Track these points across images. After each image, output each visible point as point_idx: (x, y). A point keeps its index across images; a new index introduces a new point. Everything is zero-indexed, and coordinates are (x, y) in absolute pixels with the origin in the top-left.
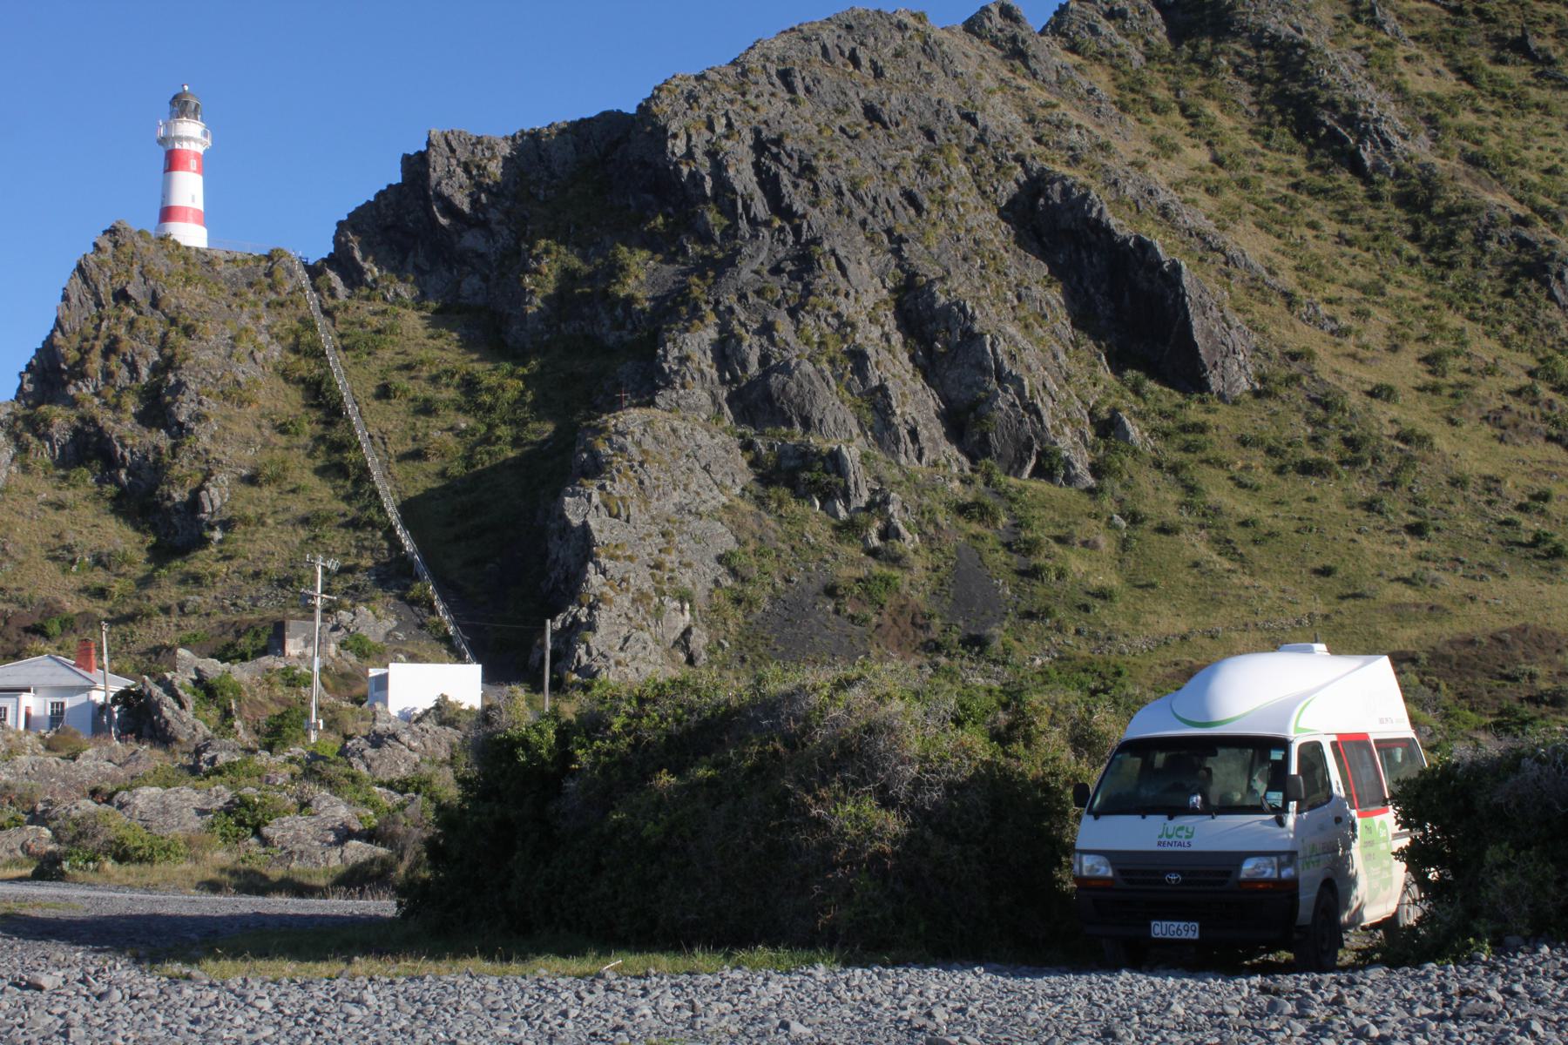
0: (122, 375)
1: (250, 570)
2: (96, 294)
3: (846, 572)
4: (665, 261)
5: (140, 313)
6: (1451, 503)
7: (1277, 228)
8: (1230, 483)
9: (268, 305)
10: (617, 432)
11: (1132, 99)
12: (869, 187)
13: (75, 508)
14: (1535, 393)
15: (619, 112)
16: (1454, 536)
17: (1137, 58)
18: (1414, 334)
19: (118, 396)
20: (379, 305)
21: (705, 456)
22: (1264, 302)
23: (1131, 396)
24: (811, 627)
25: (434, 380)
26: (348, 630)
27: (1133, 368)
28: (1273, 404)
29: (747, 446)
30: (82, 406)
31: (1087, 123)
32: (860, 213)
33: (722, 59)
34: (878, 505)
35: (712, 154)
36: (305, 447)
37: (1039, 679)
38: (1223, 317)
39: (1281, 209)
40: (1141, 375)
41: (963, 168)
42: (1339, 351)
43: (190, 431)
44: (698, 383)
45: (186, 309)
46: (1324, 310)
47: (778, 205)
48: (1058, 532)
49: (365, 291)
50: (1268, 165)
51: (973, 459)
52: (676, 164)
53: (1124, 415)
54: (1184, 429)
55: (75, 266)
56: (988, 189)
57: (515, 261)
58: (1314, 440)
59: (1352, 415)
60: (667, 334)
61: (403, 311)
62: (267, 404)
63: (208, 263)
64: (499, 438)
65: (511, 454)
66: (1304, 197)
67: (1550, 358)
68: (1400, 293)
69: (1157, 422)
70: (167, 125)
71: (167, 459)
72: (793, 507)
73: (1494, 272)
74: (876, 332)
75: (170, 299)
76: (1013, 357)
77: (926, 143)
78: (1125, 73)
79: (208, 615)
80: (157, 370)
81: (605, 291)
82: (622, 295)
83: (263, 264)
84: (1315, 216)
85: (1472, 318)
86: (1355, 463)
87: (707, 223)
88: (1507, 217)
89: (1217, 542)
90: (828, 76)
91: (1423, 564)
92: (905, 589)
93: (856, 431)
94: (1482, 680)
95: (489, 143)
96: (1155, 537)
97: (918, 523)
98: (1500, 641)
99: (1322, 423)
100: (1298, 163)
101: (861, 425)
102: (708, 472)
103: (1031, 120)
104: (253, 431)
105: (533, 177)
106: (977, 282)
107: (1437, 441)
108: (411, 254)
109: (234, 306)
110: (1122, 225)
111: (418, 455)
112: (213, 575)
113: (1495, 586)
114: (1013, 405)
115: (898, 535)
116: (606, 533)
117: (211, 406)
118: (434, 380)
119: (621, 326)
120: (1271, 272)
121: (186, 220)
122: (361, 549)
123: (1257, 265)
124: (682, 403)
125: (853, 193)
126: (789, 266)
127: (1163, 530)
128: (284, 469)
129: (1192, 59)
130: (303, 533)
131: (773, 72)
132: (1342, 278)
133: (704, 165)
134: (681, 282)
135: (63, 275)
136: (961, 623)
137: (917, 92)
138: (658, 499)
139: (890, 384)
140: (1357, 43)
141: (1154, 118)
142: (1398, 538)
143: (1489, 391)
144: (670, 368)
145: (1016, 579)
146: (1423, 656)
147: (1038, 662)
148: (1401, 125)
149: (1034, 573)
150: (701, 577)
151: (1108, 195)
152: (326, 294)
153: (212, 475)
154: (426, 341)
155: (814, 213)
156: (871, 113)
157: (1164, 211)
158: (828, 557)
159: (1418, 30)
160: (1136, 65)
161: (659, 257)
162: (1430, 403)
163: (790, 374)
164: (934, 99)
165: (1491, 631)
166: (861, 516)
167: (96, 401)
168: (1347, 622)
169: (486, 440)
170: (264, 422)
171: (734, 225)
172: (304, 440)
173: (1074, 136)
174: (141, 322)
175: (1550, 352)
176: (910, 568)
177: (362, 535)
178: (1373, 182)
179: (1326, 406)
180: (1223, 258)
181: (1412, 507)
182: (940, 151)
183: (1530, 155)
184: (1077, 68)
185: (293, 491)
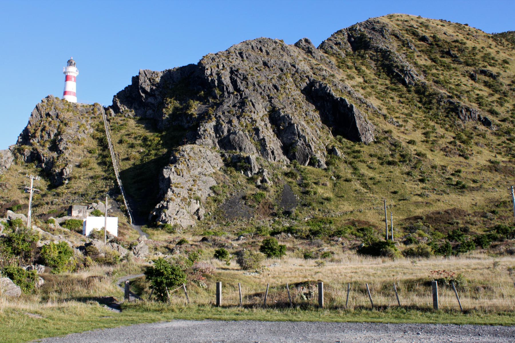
0: (46, 137)
1: (74, 192)
2: (41, 114)
3: (250, 192)
4: (203, 104)
5: (53, 119)
6: (432, 173)
7: (381, 98)
8: (367, 167)
10: (182, 151)
11: (342, 64)
12: (262, 84)
14: (455, 143)
16: (433, 182)
17: (343, 55)
18: (421, 127)
19: (44, 143)
20: (123, 118)
21: (209, 158)
22: (378, 117)
23: (338, 143)
24: (237, 209)
25: (135, 138)
27: (339, 135)
28: (379, 145)
29: (223, 156)
31: (328, 69)
32: (260, 90)
33: (223, 50)
34: (260, 173)
35: (218, 74)
36: (96, 157)
37: (306, 224)
38: (365, 120)
39: (383, 94)
40: (341, 137)
41: (291, 79)
42: (399, 131)
43: (63, 152)
46: (395, 120)
47: (236, 88)
48: (315, 181)
49: (120, 114)
50: (380, 83)
51: (291, 160)
52: (207, 77)
53: (336, 148)
54: (354, 152)
56: (298, 85)
57: (162, 105)
58: (392, 155)
59: (403, 148)
61: (129, 120)
65: (153, 158)
66: (389, 91)
67: (459, 134)
68: (416, 116)
69: (346, 150)
70: (66, 68)
71: (56, 160)
72: (235, 173)
73: (443, 111)
74: (263, 123)
75: (62, 116)
76: (303, 130)
77: (281, 72)
78: (340, 59)
80: (56, 135)
81: (185, 112)
84: (393, 96)
85: (437, 123)
86: (404, 161)
87: (215, 93)
88: (446, 96)
89: (363, 184)
90: (253, 54)
91: (424, 190)
92: (267, 197)
93: (255, 151)
94: (442, 224)
96: (344, 183)
97: (273, 178)
98: (447, 213)
99: (394, 150)
100: (388, 82)
101: (257, 150)
103: (312, 68)
104: (81, 152)
105: (168, 82)
106: (294, 110)
107: (428, 156)
110: (337, 95)
111: (128, 159)
112: (63, 193)
113: (445, 196)
114: (303, 144)
115: (266, 182)
116: (175, 180)
117: (70, 146)
118: (135, 138)
119: (189, 122)
120: (380, 109)
121: (70, 94)
122: (106, 186)
123: (376, 107)
125: (258, 85)
126: (238, 105)
127: (347, 180)
128: (89, 163)
129: (359, 55)
130: (91, 181)
131: (237, 53)
132: (400, 112)
133: (215, 77)
135: (32, 109)
136: (283, 207)
137: (279, 59)
139: (266, 138)
140: (404, 52)
141: (348, 70)
142: (417, 183)
143: (442, 143)
145: (301, 195)
146: (424, 217)
147: (306, 219)
148: (416, 72)
149: (307, 193)
150: (204, 193)
151: (334, 88)
155: (247, 91)
156: (265, 64)
157: (349, 92)
158: (244, 188)
159: (421, 49)
160: (343, 57)
161: (202, 103)
162: (425, 145)
163: (236, 134)
164: (284, 61)
165: (444, 210)
166: (256, 176)
167: (38, 144)
168: (401, 207)
169: (147, 155)
171: (223, 94)
172: (96, 155)
173: (324, 73)
174: (53, 122)
175: (459, 132)
176: (269, 191)
177: (107, 182)
178: (408, 87)
179: (395, 146)
180: (366, 105)
181: (421, 174)
182: (285, 74)
183: (452, 81)
184: (327, 57)
185: (90, 169)
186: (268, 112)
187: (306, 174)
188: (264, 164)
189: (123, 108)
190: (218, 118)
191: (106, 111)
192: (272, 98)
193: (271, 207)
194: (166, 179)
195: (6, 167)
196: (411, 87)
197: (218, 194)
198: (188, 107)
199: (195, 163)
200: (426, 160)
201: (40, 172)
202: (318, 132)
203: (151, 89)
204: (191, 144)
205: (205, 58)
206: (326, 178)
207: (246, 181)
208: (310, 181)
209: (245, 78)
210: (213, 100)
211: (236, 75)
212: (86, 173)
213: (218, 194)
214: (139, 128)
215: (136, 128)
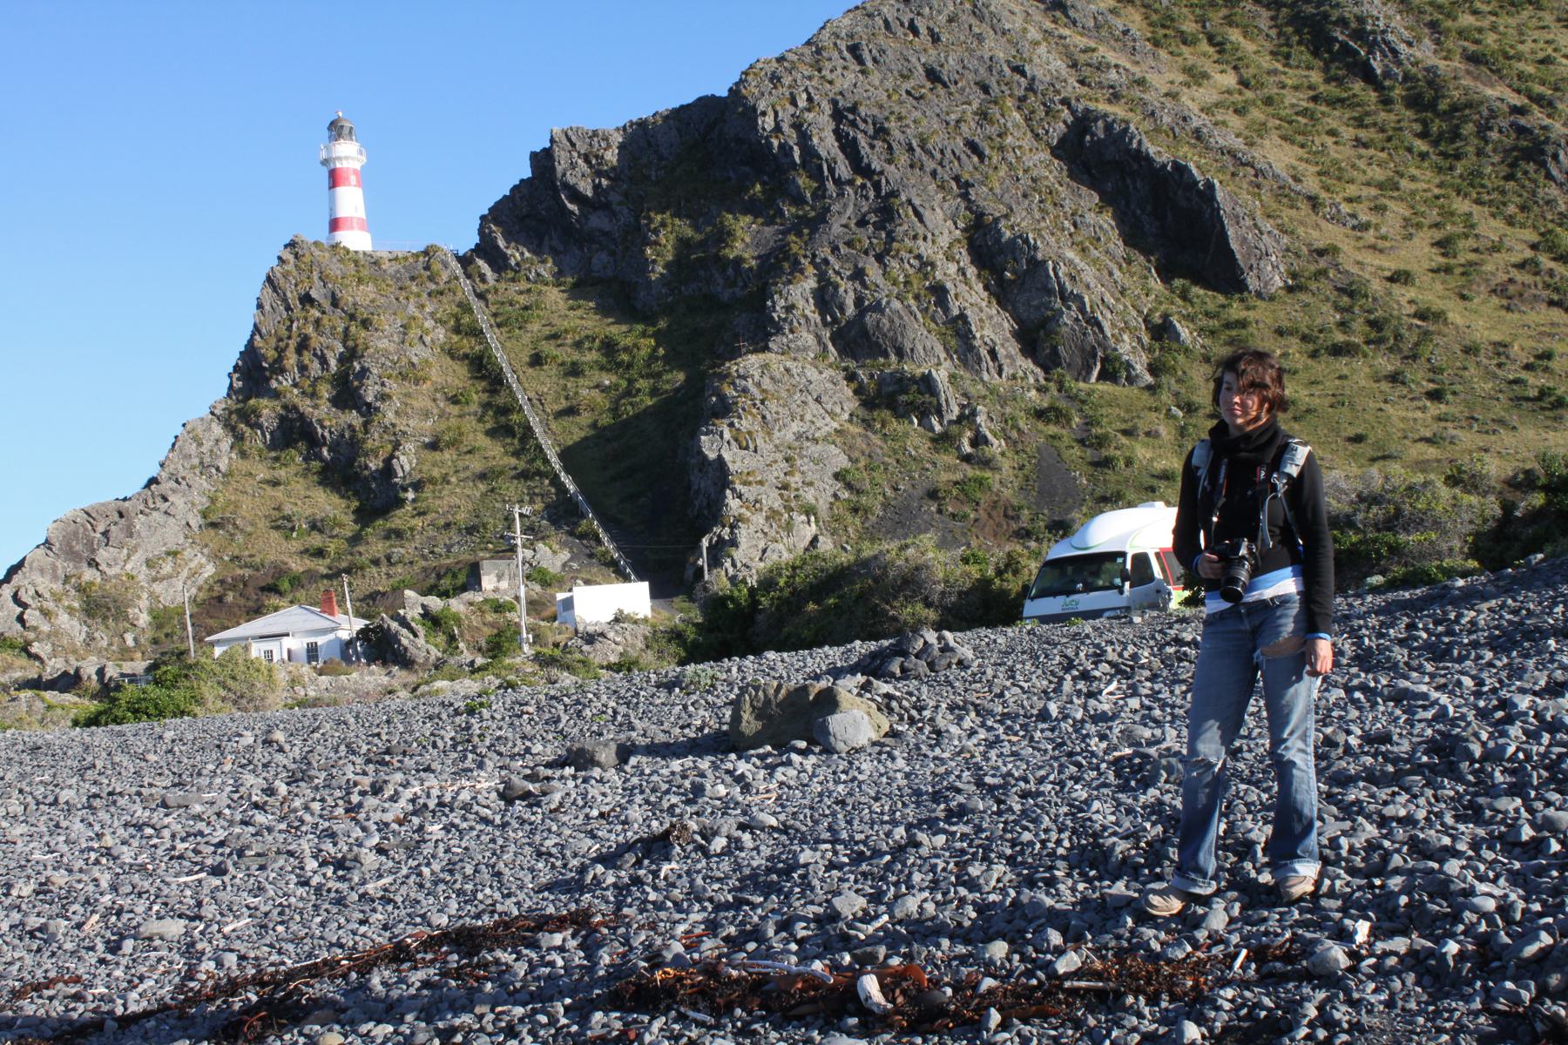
1: (442, 522)
2: (285, 300)
3: (945, 477)
4: (766, 224)
6: (1465, 368)
7: (1300, 138)
9: (429, 295)
10: (739, 377)
12: (936, 142)
14: (1537, 264)
18: (1426, 222)
19: (313, 385)
20: (524, 285)
22: (1292, 207)
23: (1179, 302)
25: (578, 345)
27: (1180, 277)
29: (851, 377)
32: (930, 165)
35: (797, 126)
36: (475, 414)
38: (1255, 225)
39: (1303, 120)
40: (1187, 283)
41: (1016, 115)
42: (1361, 243)
43: (377, 409)
46: (1345, 208)
48: (1124, 426)
49: (510, 274)
51: (1046, 370)
52: (767, 138)
53: (1174, 320)
56: (1041, 131)
57: (637, 236)
58: (1342, 325)
59: (1375, 299)
61: (544, 288)
64: (639, 390)
66: (1324, 108)
67: (1550, 232)
68: (1413, 186)
69: (1203, 322)
72: (895, 425)
73: (1496, 159)
74: (952, 268)
76: (1073, 278)
77: (983, 96)
78: (1156, 11)
80: (342, 360)
81: (717, 255)
84: (1334, 124)
85: (1478, 202)
86: (1379, 341)
91: (1443, 424)
92: (996, 486)
93: (943, 355)
97: (1003, 430)
99: (1349, 310)
100: (1316, 77)
101: (947, 350)
103: (1074, 65)
104: (430, 404)
106: (1037, 216)
107: (1450, 315)
110: (1159, 151)
111: (571, 411)
112: (412, 529)
114: (1077, 320)
115: (986, 442)
116: (739, 463)
117: (393, 386)
118: (578, 345)
119: (734, 284)
120: (1296, 179)
121: (351, 228)
123: (1284, 174)
125: (922, 148)
126: (873, 218)
130: (482, 487)
132: (1361, 178)
133: (791, 136)
135: (255, 287)
137: (971, 51)
139: (968, 312)
141: (1185, 50)
142: (1420, 404)
145: (1090, 470)
148: (1406, 34)
149: (1106, 463)
150: (821, 493)
151: (1148, 125)
156: (933, 75)
161: (760, 220)
163: (882, 312)
164: (986, 56)
166: (954, 429)
167: (296, 391)
169: (628, 393)
170: (438, 395)
171: (822, 187)
172: (474, 407)
174: (325, 321)
175: (1550, 226)
176: (999, 469)
178: (1384, 88)
179: (1351, 294)
181: (1431, 375)
182: (996, 103)
185: (470, 452)
186: (964, 230)
187: (1095, 407)
188: (972, 391)
189: (515, 254)
190: (821, 267)
191: (464, 267)
192: (968, 185)
193: (1010, 513)
194: (710, 463)
195: (218, 469)
196: (1392, 88)
197: (859, 492)
198: (723, 236)
200: (1445, 330)
201: (319, 473)
202: (1117, 273)
203: (596, 187)
205: (750, 78)
206: (1154, 415)
207: (929, 444)
208: (1108, 428)
209: (881, 132)
210: (793, 210)
211: (853, 124)
212: (460, 464)
213: (859, 492)
214: (579, 312)
215: (571, 313)
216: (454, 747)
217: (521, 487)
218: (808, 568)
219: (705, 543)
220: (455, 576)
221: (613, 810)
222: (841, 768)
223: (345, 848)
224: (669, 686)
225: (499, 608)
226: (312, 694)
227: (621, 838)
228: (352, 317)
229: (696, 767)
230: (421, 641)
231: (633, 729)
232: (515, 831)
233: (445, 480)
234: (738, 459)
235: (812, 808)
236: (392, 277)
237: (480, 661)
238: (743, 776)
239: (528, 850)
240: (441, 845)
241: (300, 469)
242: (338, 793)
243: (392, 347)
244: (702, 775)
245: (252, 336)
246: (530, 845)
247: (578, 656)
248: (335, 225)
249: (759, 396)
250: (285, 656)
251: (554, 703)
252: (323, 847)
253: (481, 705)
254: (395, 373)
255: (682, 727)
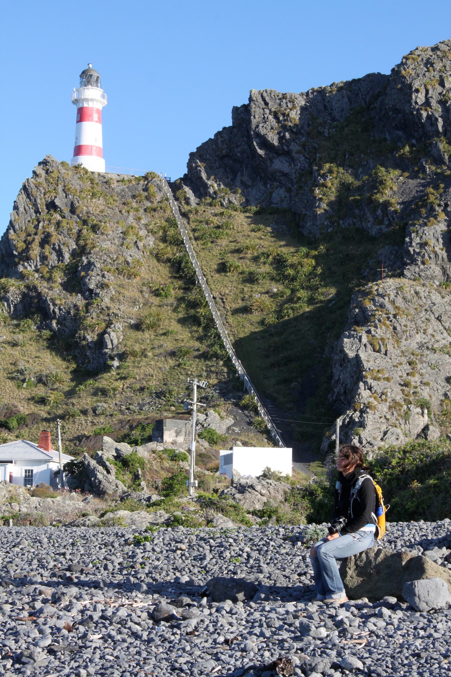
1: (138, 386)
2: (35, 205)
9: (145, 210)
10: (378, 295)
13: (24, 345)
15: (379, 74)
19: (50, 272)
20: (218, 209)
25: (256, 259)
26: (203, 426)
30: (28, 279)
43: (97, 295)
44: (433, 261)
45: (93, 214)
49: (209, 200)
52: (418, 110)
55: (21, 187)
60: (412, 228)
61: (234, 213)
62: (147, 277)
63: (106, 182)
64: (299, 298)
71: (82, 314)
79: (111, 415)
80: (74, 254)
82: (381, 201)
83: (142, 182)
87: (439, 150)
95: (291, 98)
102: (440, 321)
104: (137, 294)
105: (320, 120)
108: (239, 174)
109: (123, 211)
112: (114, 389)
116: (372, 363)
117: (110, 278)
119: (381, 222)
121: (91, 154)
124: (423, 274)
128: (159, 320)
130: (172, 362)
134: (421, 191)
138: (406, 340)
144: (414, 250)
152: (183, 202)
153: (112, 324)
154: (250, 233)
161: (406, 174)
167: (36, 275)
169: (290, 300)
170: (145, 288)
172: (171, 300)
174: (64, 224)
185: (164, 334)
194: (349, 360)
199: (408, 323)
201: (48, 340)
203: (281, 138)
204: (393, 276)
205: (409, 62)
210: (433, 168)
212: (156, 343)
214: (259, 234)
216: (121, 570)
217: (202, 364)
218: (416, 454)
219: (339, 422)
220: (143, 429)
221: (236, 638)
222: (421, 625)
223: (24, 646)
224: (294, 540)
225: (174, 457)
226: (24, 510)
227: (238, 664)
228: (85, 222)
229: (306, 610)
230: (112, 477)
231: (261, 572)
232: (157, 647)
233: (144, 354)
234: (371, 359)
235: (393, 657)
236: (119, 194)
237: (155, 498)
238: (341, 622)
239: (165, 664)
240: (98, 651)
241: (34, 335)
242: (26, 599)
243: (113, 248)
244: (310, 617)
245: (8, 230)
246: (166, 660)
247: (231, 502)
248: (78, 150)
249: (393, 312)
250: (8, 479)
251: (202, 543)
252: (7, 643)
253: (146, 539)
254: (113, 268)
255: (300, 575)
